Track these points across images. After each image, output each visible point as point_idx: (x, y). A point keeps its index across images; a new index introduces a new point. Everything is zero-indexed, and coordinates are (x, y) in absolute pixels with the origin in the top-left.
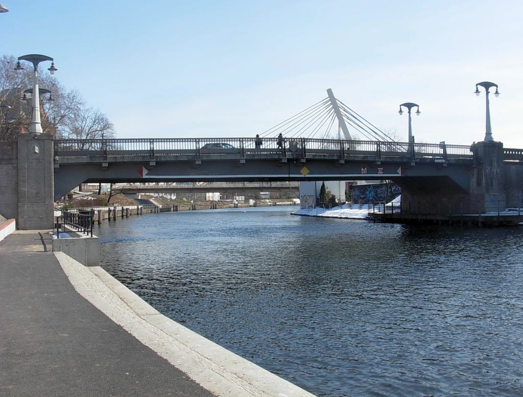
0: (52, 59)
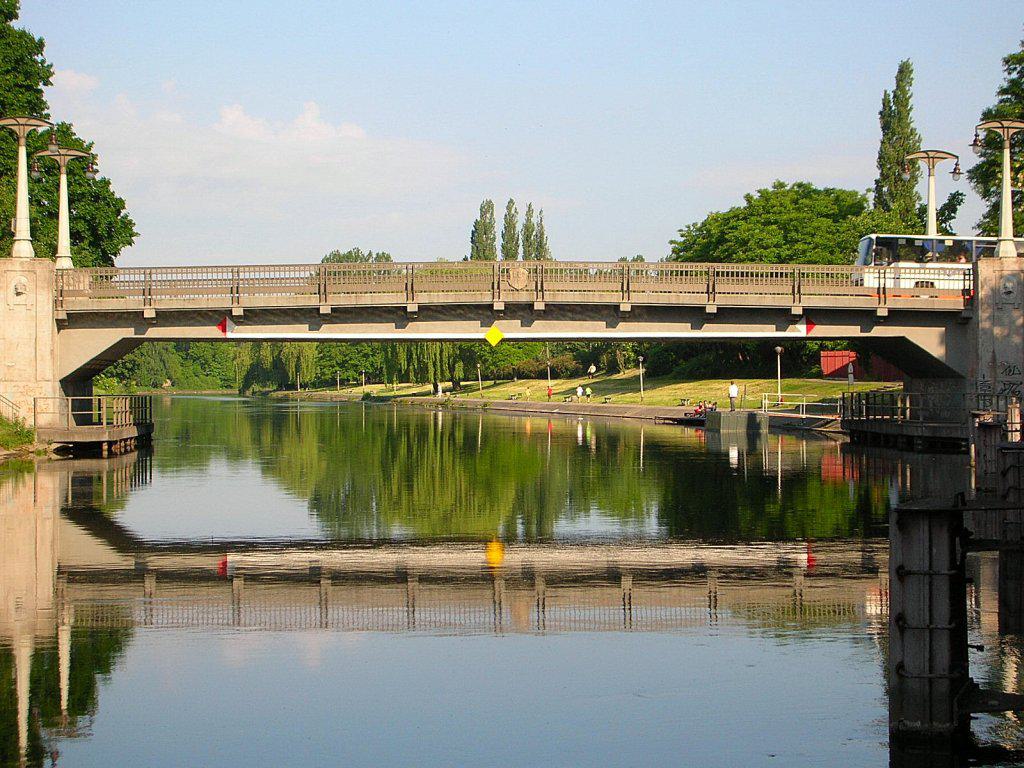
0: (957, 157)
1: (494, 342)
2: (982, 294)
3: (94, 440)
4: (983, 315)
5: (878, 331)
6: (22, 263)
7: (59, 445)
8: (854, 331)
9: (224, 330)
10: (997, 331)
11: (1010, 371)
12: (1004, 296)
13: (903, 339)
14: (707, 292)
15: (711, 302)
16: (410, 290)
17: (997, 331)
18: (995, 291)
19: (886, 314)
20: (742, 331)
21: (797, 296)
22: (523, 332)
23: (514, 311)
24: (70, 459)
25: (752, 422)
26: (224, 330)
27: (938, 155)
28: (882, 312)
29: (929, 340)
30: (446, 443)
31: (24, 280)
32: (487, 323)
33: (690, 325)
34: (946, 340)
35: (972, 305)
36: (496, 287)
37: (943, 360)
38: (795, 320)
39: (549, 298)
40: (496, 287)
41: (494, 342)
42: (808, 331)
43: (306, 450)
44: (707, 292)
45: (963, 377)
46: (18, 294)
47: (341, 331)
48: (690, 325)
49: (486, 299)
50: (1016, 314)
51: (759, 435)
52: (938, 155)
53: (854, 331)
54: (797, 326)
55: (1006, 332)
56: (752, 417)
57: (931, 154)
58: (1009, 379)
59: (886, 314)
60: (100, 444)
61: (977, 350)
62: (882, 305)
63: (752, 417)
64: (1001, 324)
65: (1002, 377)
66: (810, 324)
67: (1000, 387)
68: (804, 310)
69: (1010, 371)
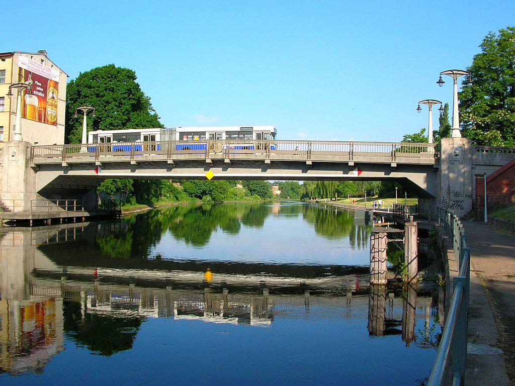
0: (441, 103)
1: (210, 178)
2: (443, 157)
3: (24, 218)
4: (444, 167)
5: (393, 175)
6: (15, 143)
7: (8, 220)
8: (381, 174)
9: (97, 172)
10: (451, 175)
11: (457, 195)
12: (454, 157)
13: (406, 179)
14: (131, 155)
15: (308, 159)
16: (169, 154)
17: (451, 175)
18: (450, 155)
19: (396, 166)
20: (326, 174)
21: (394, 158)
22: (223, 173)
23: (217, 163)
24: (15, 226)
25: (367, 215)
26: (97, 172)
27: (433, 102)
28: (394, 165)
29: (419, 179)
30: (332, 216)
31: (15, 150)
32: (207, 169)
33: (301, 171)
34: (427, 180)
35: (439, 162)
36: (393, 155)
37: (426, 190)
38: (352, 168)
39: (231, 157)
40: (393, 155)
41: (210, 178)
42: (359, 174)
43: (312, 214)
44: (96, 156)
45: (435, 198)
46: (13, 156)
47: (108, 173)
48: (301, 171)
49: (202, 157)
50: (461, 166)
51: (369, 220)
52: (433, 102)
53: (381, 174)
54: (353, 172)
55: (456, 175)
56: (367, 213)
57: (430, 101)
58: (456, 199)
59: (396, 166)
60: (73, 217)
61: (441, 184)
62: (351, 160)
63: (367, 213)
64: (454, 172)
65: (453, 198)
66: (360, 171)
67: (452, 203)
68: (397, 165)
69: (457, 195)
